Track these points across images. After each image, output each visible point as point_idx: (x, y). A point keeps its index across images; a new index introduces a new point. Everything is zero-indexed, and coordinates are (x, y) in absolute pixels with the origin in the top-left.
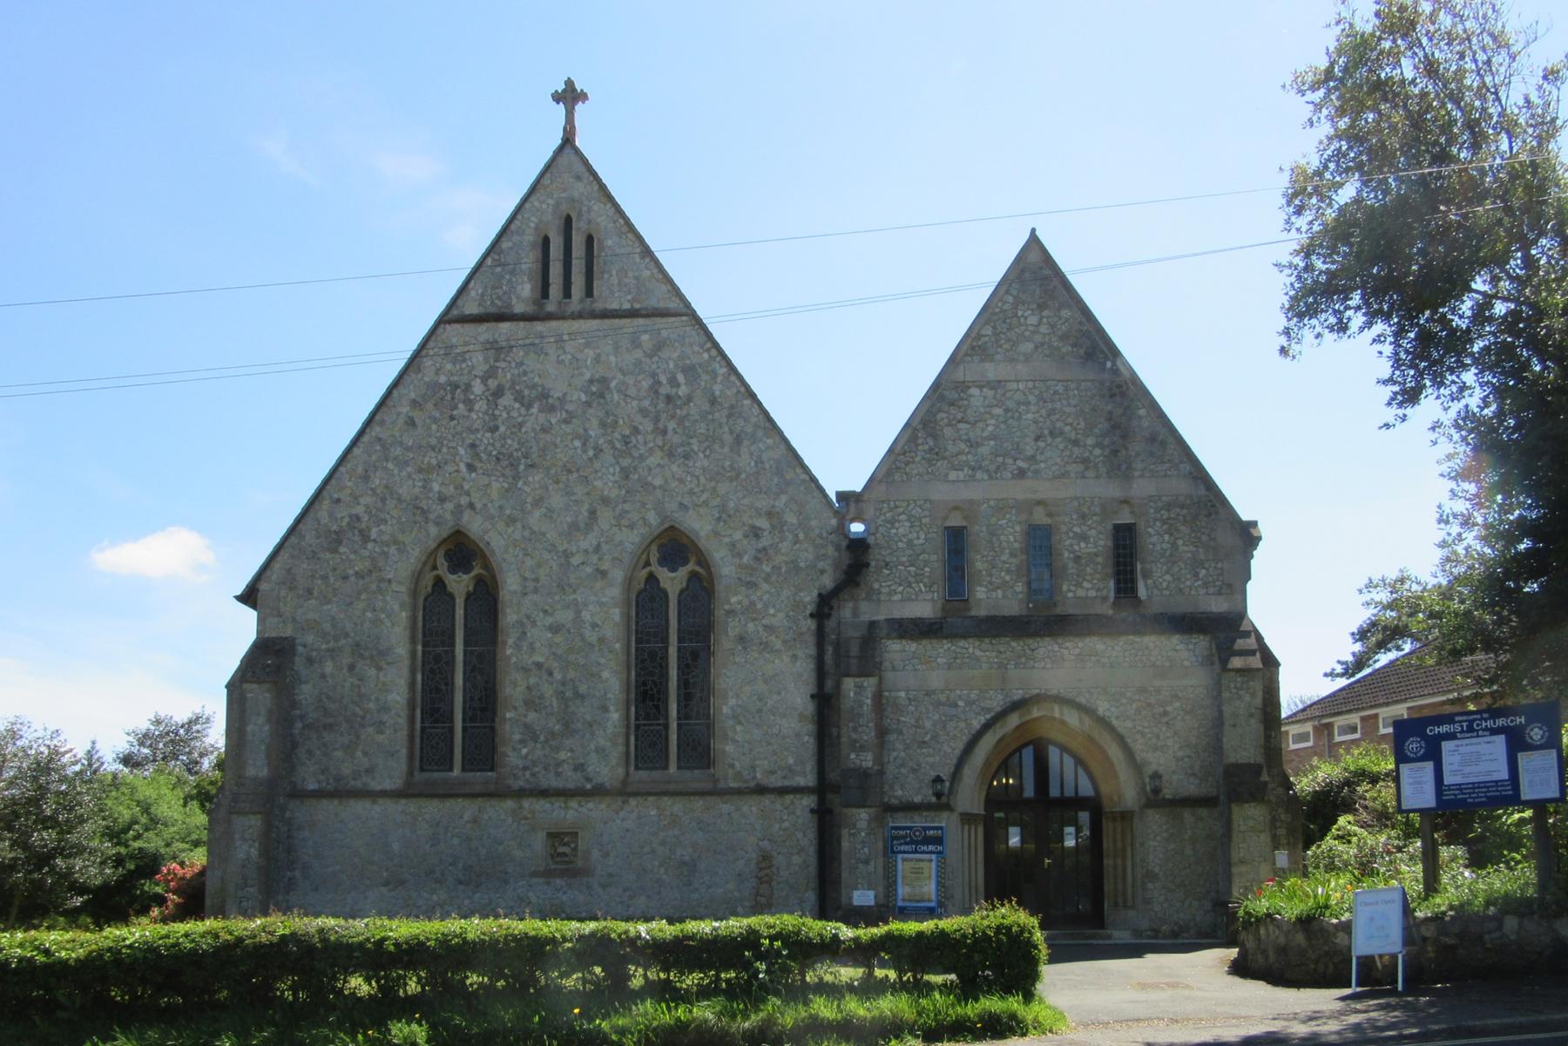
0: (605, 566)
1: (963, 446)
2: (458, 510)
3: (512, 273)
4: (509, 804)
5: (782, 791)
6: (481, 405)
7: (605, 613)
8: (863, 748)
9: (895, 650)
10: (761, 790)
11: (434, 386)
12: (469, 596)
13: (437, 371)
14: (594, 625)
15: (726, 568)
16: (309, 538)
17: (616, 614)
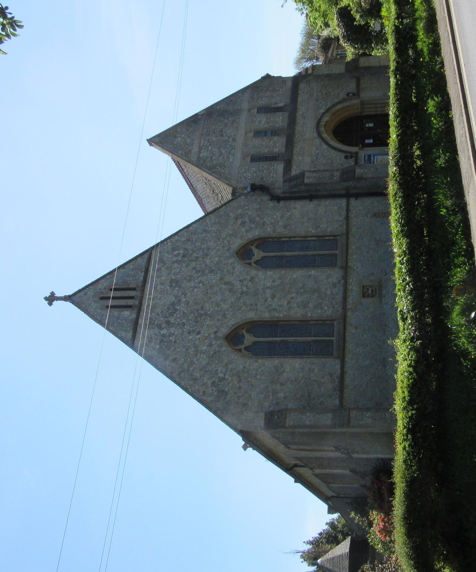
1: (221, 158)
2: (216, 338)
4: (349, 313)
5: (348, 210)
10: (347, 218)
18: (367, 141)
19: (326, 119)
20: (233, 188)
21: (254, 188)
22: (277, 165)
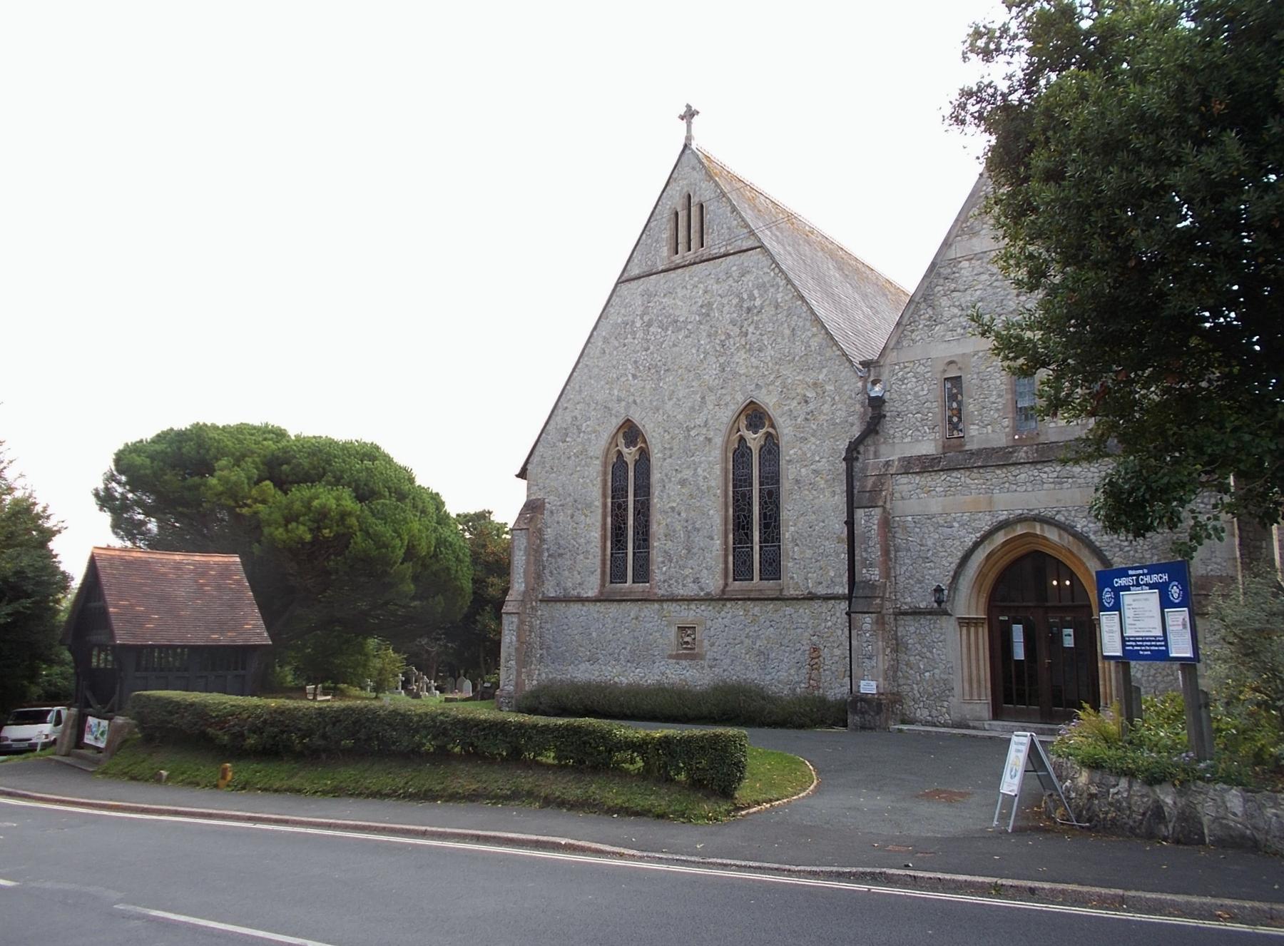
0: (711, 435)
1: (956, 311)
2: (627, 407)
3: (657, 241)
4: (656, 606)
5: (827, 598)
6: (640, 334)
7: (711, 470)
8: (871, 565)
9: (905, 484)
10: (812, 597)
11: (616, 325)
12: (636, 462)
13: (615, 318)
14: (705, 478)
15: (786, 430)
16: (552, 435)
17: (718, 470)
18: (1018, 631)
19: (1052, 535)
20: (877, 362)
21: (877, 404)
22: (935, 440)
